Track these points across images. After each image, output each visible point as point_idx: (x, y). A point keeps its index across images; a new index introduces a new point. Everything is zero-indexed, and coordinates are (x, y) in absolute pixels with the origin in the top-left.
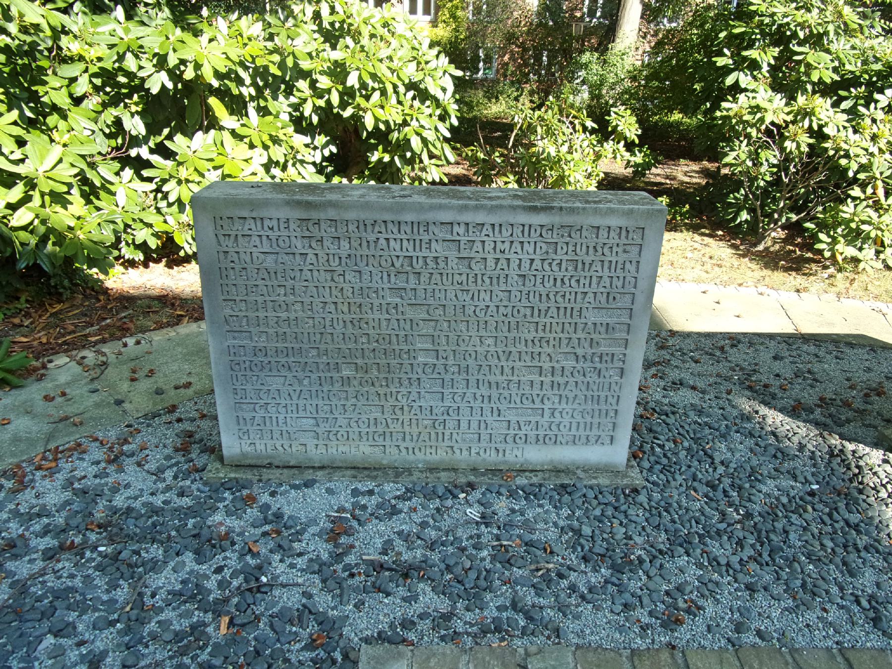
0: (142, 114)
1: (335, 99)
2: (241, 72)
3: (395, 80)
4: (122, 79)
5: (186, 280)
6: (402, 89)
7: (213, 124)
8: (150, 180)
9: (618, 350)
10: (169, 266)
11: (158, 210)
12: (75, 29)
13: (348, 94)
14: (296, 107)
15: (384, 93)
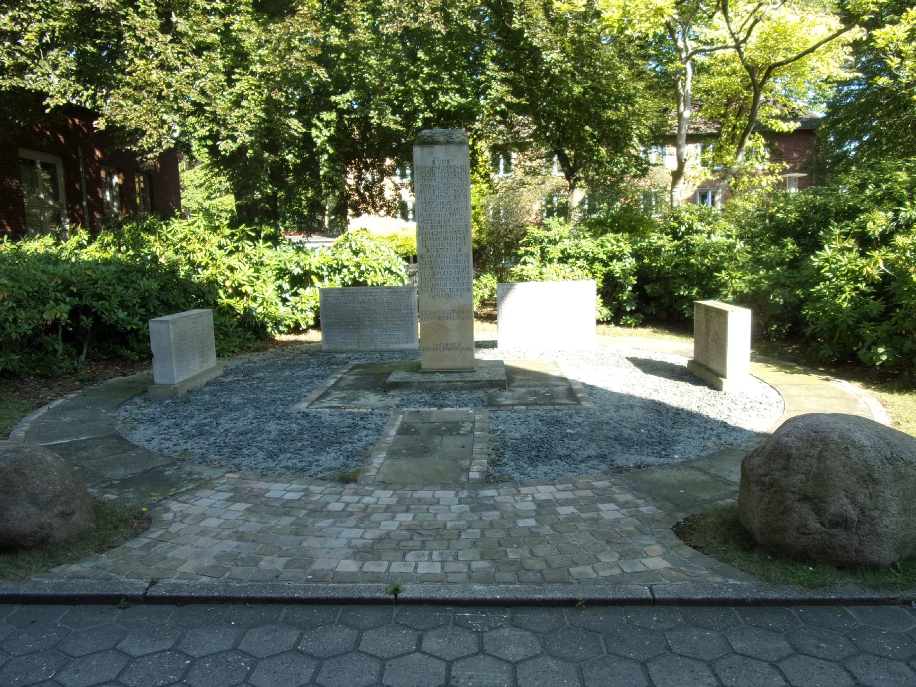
1: (357, 275)
13: (362, 273)
14: (343, 279)
15: (375, 272)
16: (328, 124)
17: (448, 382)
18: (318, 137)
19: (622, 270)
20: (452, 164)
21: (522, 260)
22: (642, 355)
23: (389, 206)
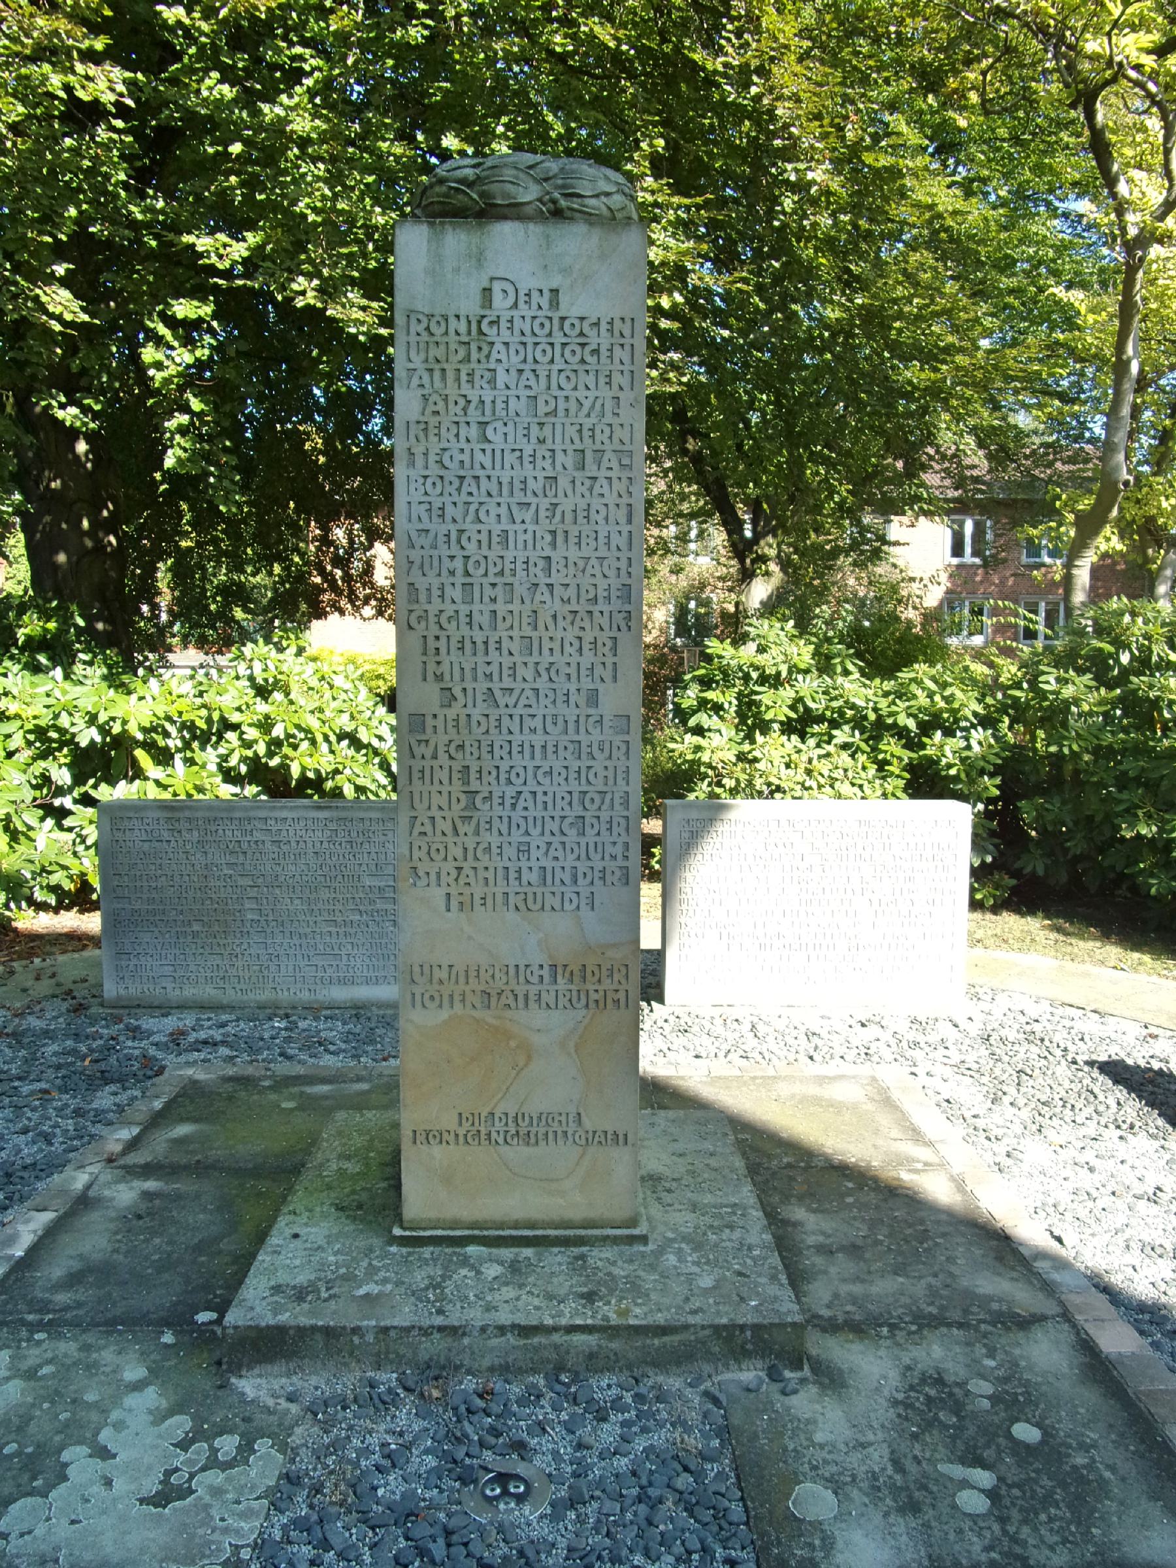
0: (69, 766)
1: (261, 749)
2: (168, 726)
3: (326, 730)
4: (54, 735)
5: (92, 923)
6: (333, 738)
7: (138, 774)
8: (70, 829)
9: (390, 907)
10: (81, 912)
11: (75, 854)
12: (15, 692)
13: (275, 745)
14: (225, 758)
15: (313, 742)
16: (188, 331)
17: (525, 1331)
18: (159, 366)
19: (963, 760)
20: (574, 306)
21: (692, 723)
22: (1137, 1056)
23: (383, 599)
